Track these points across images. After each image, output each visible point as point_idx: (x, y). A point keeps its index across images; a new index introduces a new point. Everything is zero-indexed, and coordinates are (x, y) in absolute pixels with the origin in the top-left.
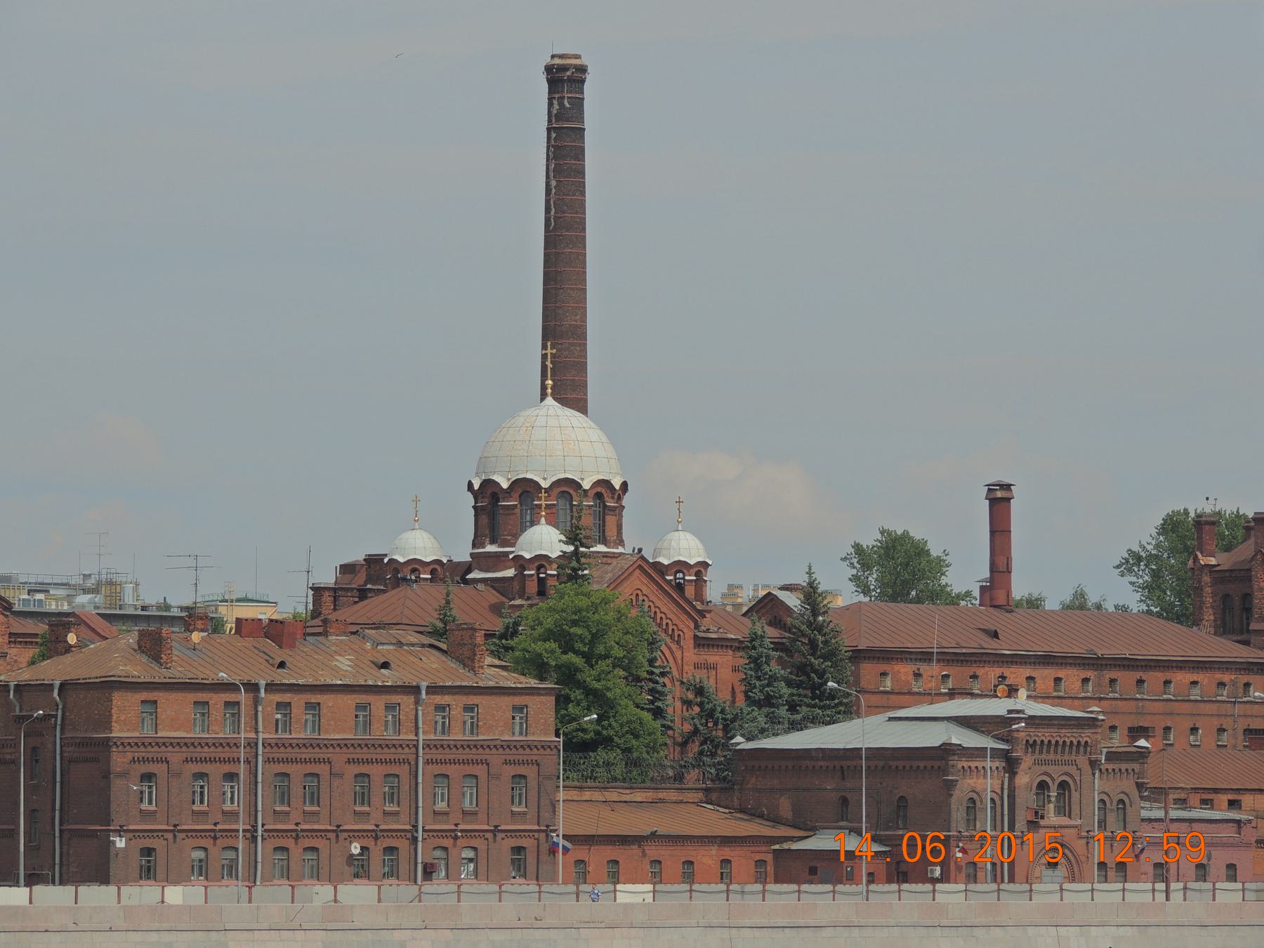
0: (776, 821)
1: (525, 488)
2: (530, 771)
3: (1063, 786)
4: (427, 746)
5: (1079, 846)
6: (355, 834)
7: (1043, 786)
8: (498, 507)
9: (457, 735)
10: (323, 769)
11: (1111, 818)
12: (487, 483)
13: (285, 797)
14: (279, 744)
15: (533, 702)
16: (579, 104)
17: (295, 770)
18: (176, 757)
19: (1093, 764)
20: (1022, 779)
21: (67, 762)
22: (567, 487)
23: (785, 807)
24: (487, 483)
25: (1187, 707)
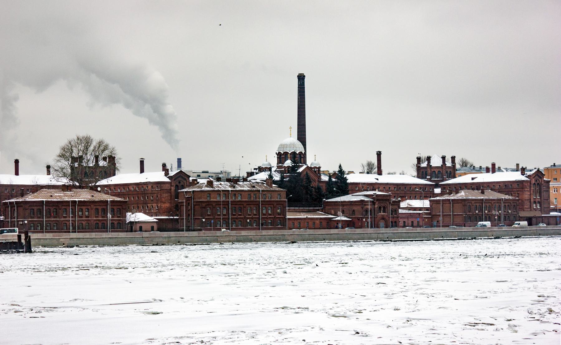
0: (332, 215)
1: (286, 153)
2: (242, 206)
3: (384, 207)
4: (262, 201)
5: (387, 218)
6: (248, 218)
7: (380, 208)
8: (281, 157)
9: (252, 199)
10: (242, 206)
11: (393, 213)
12: (279, 153)
13: (235, 210)
14: (264, 201)
15: (282, 193)
16: (304, 83)
17: (507, 204)
18: (245, 204)
19: (390, 203)
20: (376, 206)
21: (194, 205)
22: (294, 153)
23: (333, 212)
24: (279, 153)
25: (414, 192)
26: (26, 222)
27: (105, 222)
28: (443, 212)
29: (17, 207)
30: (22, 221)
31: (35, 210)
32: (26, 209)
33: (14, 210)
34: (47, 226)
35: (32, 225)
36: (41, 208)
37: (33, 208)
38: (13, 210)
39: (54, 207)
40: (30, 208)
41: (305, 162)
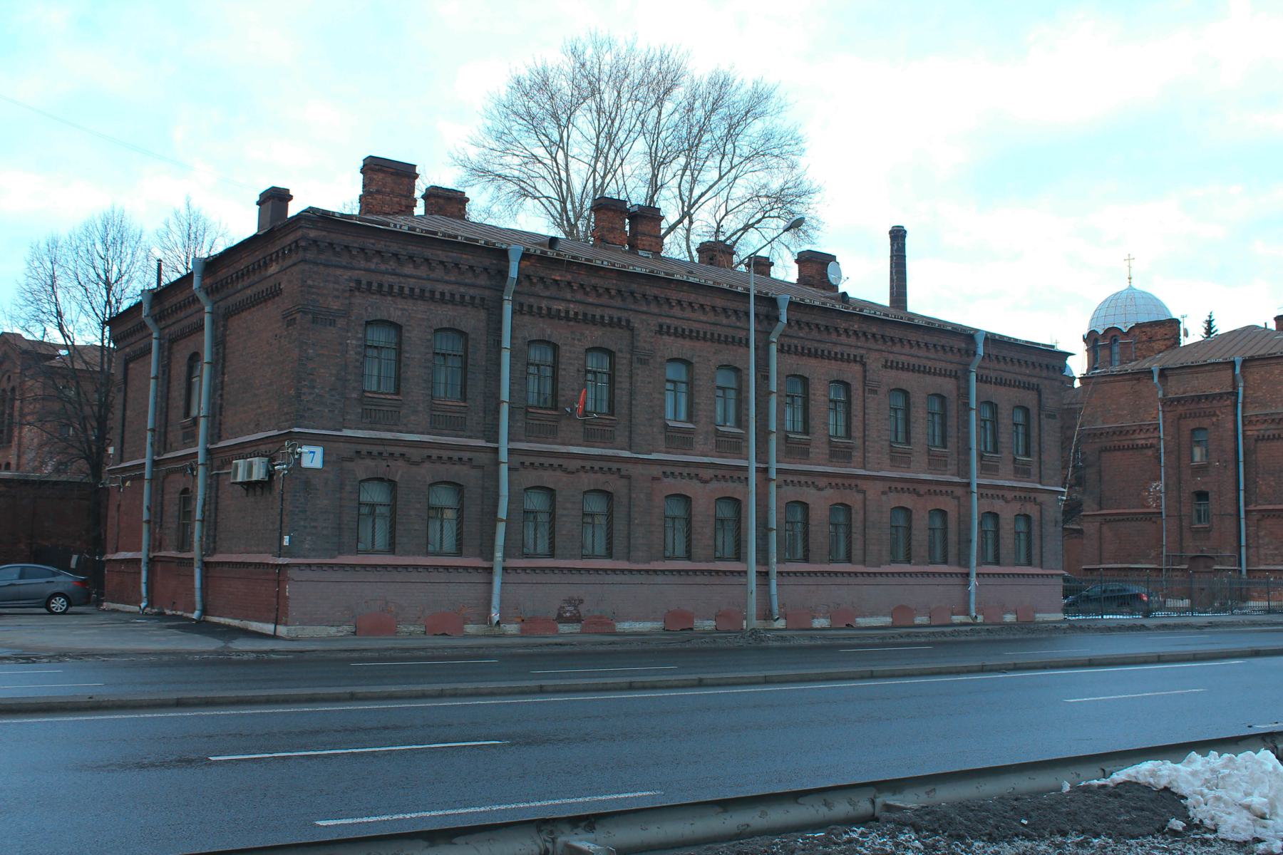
26: (312, 458)
27: (949, 505)
28: (211, 544)
29: (223, 318)
30: (270, 450)
31: (414, 335)
32: (322, 318)
33: (195, 358)
34: (522, 515)
35: (375, 494)
36: (472, 321)
37: (393, 310)
38: (179, 368)
39: (595, 335)
40: (367, 306)
41: (1074, 378)
